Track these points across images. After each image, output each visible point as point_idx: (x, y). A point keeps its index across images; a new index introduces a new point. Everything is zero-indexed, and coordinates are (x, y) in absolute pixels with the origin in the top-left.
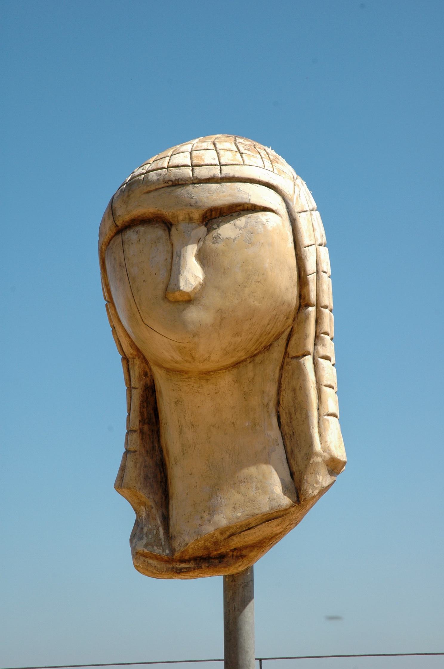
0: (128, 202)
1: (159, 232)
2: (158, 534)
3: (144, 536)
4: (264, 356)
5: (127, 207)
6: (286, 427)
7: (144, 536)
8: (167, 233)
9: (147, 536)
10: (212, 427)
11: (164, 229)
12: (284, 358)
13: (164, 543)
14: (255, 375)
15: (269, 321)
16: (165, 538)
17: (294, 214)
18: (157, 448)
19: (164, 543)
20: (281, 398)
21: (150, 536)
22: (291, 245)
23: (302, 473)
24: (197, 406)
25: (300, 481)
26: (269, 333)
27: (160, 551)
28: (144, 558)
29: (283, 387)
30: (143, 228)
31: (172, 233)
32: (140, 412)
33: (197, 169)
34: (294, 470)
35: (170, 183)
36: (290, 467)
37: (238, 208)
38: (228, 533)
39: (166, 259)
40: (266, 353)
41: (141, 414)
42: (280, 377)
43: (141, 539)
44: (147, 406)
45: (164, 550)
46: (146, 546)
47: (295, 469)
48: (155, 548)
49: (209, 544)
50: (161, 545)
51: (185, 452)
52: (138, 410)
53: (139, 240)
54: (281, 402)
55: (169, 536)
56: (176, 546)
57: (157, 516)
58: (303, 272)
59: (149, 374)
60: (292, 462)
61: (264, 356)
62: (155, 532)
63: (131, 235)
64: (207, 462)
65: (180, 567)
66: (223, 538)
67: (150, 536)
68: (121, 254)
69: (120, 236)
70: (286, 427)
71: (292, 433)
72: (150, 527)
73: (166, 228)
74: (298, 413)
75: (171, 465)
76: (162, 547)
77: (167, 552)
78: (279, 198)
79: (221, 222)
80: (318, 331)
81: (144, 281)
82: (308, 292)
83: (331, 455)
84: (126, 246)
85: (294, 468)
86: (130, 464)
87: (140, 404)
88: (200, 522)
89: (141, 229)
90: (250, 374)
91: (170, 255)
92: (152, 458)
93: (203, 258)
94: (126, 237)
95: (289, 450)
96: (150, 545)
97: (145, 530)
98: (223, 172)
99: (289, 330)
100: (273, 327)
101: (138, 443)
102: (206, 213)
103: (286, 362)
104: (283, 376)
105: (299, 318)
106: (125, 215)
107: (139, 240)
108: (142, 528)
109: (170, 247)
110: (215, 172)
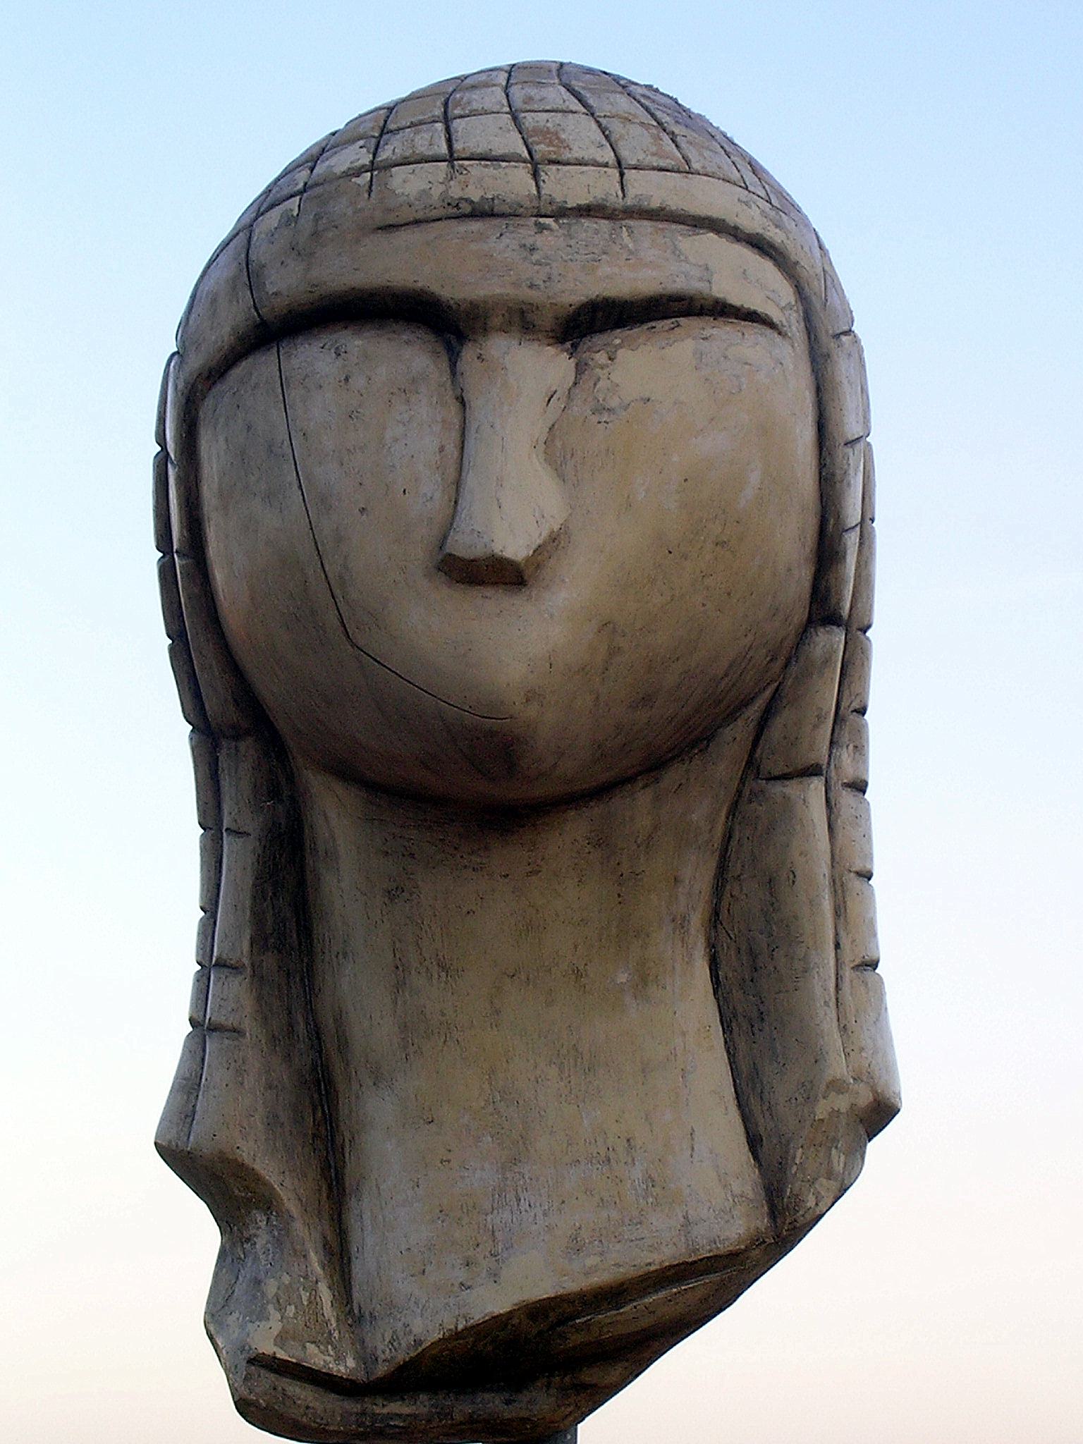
0: (312, 254)
1: (405, 357)
2: (314, 1300)
3: (270, 1308)
4: (687, 771)
5: (308, 270)
6: (737, 994)
7: (270, 1308)
8: (445, 365)
9: (281, 1309)
10: (508, 980)
11: (435, 353)
12: (742, 781)
13: (336, 1334)
14: (656, 828)
15: (730, 666)
16: (338, 1320)
17: (824, 339)
18: (301, 1028)
19: (336, 1334)
20: (725, 904)
21: (291, 1310)
22: (806, 434)
23: (788, 1142)
24: (465, 910)
25: (782, 1166)
26: (720, 702)
27: (328, 1358)
28: (272, 1376)
29: (735, 868)
30: (358, 342)
31: (461, 366)
32: (253, 913)
33: (551, 174)
34: (761, 1130)
35: (467, 209)
36: (745, 1118)
37: (676, 306)
38: (552, 1317)
39: (442, 449)
40: (696, 761)
41: (258, 918)
42: (728, 837)
43: (262, 1316)
44: (274, 894)
45: (339, 1358)
46: (281, 1339)
47: (763, 1125)
48: (311, 1348)
49: (490, 1348)
50: (329, 1341)
51: (411, 1049)
52: (248, 903)
53: (347, 379)
54: (724, 915)
55: (351, 1311)
56: (381, 1347)
57: (309, 1246)
58: (832, 521)
59: (286, 793)
60: (754, 1102)
61: (687, 771)
62: (305, 1296)
63: (314, 357)
64: (486, 1086)
65: (385, 1411)
66: (534, 1332)
67: (291, 1310)
68: (277, 415)
69: (274, 358)
70: (737, 994)
71: (755, 1014)
72: (286, 1279)
73: (440, 348)
74: (779, 954)
75: (355, 1086)
76: (334, 1348)
77: (351, 1363)
78: (786, 293)
79: (620, 346)
80: (844, 704)
81: (363, 510)
82: (841, 581)
83: (875, 1092)
84: (294, 394)
85: (761, 1121)
86: (216, 1074)
87: (254, 885)
88: (461, 1275)
89: (356, 342)
90: (644, 822)
91: (455, 435)
92: (288, 1057)
93: (557, 452)
94: (295, 362)
95: (744, 1067)
96: (294, 1339)
97: (271, 1288)
98: (631, 192)
99: (768, 693)
100: (734, 685)
101: (248, 1010)
102: (579, 315)
103: (746, 792)
104: (736, 836)
105: (802, 659)
106: (286, 283)
107: (347, 379)
108: (257, 1282)
109: (454, 407)
110: (602, 186)
